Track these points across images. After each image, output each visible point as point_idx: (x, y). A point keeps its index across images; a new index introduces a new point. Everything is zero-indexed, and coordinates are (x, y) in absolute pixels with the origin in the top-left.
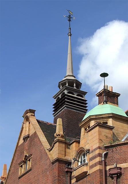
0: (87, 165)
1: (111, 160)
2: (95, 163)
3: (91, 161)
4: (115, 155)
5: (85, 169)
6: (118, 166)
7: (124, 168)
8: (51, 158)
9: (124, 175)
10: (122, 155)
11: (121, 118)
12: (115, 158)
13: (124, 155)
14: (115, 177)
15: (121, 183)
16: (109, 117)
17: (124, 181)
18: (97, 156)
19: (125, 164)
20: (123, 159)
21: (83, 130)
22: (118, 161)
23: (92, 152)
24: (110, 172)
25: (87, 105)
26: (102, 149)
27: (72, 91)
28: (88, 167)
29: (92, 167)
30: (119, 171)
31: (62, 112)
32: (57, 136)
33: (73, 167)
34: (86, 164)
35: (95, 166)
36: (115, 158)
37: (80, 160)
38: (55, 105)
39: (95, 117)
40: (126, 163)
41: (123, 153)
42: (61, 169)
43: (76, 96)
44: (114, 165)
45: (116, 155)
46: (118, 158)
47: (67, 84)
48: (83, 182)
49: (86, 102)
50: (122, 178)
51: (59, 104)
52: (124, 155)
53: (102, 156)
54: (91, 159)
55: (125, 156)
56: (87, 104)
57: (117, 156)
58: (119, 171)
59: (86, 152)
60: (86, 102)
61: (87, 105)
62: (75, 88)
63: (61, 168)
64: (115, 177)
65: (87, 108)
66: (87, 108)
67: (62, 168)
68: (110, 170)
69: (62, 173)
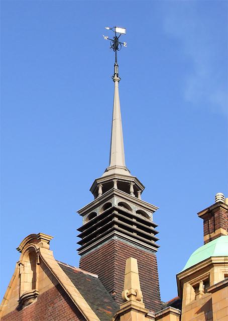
43: (134, 214)
47: (115, 186)
62: (134, 196)
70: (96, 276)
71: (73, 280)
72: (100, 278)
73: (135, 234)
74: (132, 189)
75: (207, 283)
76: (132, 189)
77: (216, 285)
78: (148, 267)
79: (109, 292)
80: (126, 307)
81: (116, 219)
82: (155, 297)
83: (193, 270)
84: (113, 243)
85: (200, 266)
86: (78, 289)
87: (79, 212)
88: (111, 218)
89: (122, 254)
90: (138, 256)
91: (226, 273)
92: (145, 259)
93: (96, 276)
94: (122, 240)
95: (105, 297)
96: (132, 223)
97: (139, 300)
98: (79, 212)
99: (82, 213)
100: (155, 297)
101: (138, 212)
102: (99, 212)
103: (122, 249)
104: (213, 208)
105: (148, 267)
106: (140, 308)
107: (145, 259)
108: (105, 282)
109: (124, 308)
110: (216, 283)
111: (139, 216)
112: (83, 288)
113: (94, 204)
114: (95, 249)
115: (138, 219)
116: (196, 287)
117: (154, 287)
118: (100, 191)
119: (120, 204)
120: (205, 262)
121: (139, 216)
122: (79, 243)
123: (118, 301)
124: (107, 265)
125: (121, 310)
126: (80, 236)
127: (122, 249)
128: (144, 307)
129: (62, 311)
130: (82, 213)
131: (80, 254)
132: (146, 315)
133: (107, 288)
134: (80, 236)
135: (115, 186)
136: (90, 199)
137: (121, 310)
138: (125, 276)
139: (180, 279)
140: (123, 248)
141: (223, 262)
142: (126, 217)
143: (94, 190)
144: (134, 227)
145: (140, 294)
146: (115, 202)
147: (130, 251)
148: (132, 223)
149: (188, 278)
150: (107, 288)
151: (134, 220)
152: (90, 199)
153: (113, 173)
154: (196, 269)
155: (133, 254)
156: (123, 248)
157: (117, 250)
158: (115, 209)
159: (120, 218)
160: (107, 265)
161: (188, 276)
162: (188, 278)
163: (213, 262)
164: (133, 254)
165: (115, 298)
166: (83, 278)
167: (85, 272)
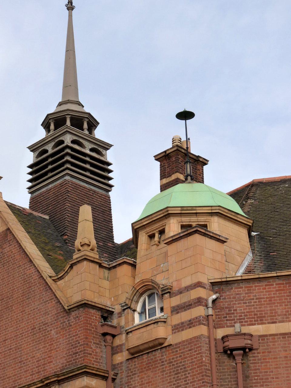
0: (165, 322)
1: (227, 314)
2: (189, 319)
3: (178, 313)
4: (235, 304)
5: (160, 332)
6: (246, 330)
7: (260, 336)
8: (63, 298)
9: (258, 353)
10: (254, 305)
11: (236, 218)
12: (236, 310)
13: (257, 305)
14: (239, 355)
15: (251, 370)
16: (212, 214)
17: (259, 366)
18: (195, 303)
19: (260, 326)
20: (255, 315)
21: (144, 238)
22: (244, 319)
23: (180, 292)
24: (226, 344)
25: (110, 175)
26: (205, 288)
27: (81, 140)
28: (170, 328)
29: (178, 328)
30: (249, 342)
31: (55, 187)
32: (81, 248)
33: (119, 324)
34: (163, 320)
35: (190, 327)
36: (236, 310)
37: (139, 308)
38: (35, 169)
39: (181, 210)
40: (262, 324)
41: (255, 302)
42: (93, 328)
43: (88, 152)
44: (234, 326)
45: (239, 304)
46: (244, 313)
47: (68, 123)
48: (150, 363)
49: (110, 167)
50: (255, 360)
51: (46, 166)
52: (257, 305)
53: (206, 306)
54: (176, 310)
55: (260, 308)
56: (110, 171)
57: (240, 308)
58: (249, 342)
59: (162, 291)
60: (110, 167)
61: (110, 175)
62: (86, 132)
63: (93, 324)
64: (239, 355)
65: (111, 182)
66: (111, 182)
67: (95, 325)
68: (225, 339)
69: (94, 337)
70: (47, 217)
71: (22, 223)
72: (51, 220)
73: (88, 174)
74: (85, 126)
75: (162, 232)
76: (85, 126)
77: (172, 237)
78: (101, 207)
79: (61, 234)
80: (79, 257)
81: (68, 158)
82: (108, 239)
83: (149, 220)
84: (65, 183)
85: (156, 216)
86: (28, 232)
87: (29, 148)
88: (62, 157)
89: (75, 195)
90: (91, 197)
91: (182, 224)
92: (99, 200)
93: (47, 217)
94: (74, 180)
95: (57, 240)
96: (85, 162)
97: (92, 250)
98: (29, 148)
99: (32, 148)
100: (108, 239)
101: (92, 150)
102: (50, 148)
103: (75, 190)
104: (170, 151)
105: (101, 207)
106: (94, 258)
107: (99, 200)
108: (55, 225)
109: (77, 258)
110: (172, 234)
111: (94, 154)
112: (33, 231)
113: (45, 140)
114: (46, 188)
115: (92, 158)
116: (152, 237)
117: (107, 229)
118: (52, 127)
119: (73, 142)
120: (161, 212)
121: (94, 154)
122: (30, 181)
123: (70, 245)
124: (59, 206)
125: (75, 260)
126: (30, 174)
127: (75, 190)
128: (98, 257)
129: (12, 257)
130: (32, 148)
131: (29, 193)
132: (100, 266)
133: (58, 231)
134: (30, 174)
135: (68, 123)
136: (41, 134)
137: (75, 260)
138: (79, 224)
139: (135, 228)
140: (76, 188)
141: (180, 212)
142: (78, 155)
143: (46, 125)
144: (88, 166)
145: (94, 242)
146: (68, 139)
147: (83, 191)
148: (85, 162)
149: (144, 227)
150: (58, 231)
151: (88, 159)
152: (41, 134)
153: (83, 254)
154: (152, 218)
155: (86, 194)
156: (76, 188)
157: (70, 190)
158: (67, 147)
159: (73, 157)
160: (59, 206)
161: (144, 225)
162: (144, 227)
163: (169, 212)
164: (86, 194)
165: (67, 241)
166: (34, 220)
167: (34, 213)
